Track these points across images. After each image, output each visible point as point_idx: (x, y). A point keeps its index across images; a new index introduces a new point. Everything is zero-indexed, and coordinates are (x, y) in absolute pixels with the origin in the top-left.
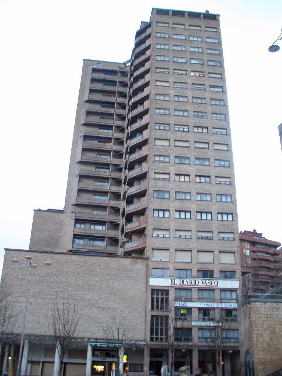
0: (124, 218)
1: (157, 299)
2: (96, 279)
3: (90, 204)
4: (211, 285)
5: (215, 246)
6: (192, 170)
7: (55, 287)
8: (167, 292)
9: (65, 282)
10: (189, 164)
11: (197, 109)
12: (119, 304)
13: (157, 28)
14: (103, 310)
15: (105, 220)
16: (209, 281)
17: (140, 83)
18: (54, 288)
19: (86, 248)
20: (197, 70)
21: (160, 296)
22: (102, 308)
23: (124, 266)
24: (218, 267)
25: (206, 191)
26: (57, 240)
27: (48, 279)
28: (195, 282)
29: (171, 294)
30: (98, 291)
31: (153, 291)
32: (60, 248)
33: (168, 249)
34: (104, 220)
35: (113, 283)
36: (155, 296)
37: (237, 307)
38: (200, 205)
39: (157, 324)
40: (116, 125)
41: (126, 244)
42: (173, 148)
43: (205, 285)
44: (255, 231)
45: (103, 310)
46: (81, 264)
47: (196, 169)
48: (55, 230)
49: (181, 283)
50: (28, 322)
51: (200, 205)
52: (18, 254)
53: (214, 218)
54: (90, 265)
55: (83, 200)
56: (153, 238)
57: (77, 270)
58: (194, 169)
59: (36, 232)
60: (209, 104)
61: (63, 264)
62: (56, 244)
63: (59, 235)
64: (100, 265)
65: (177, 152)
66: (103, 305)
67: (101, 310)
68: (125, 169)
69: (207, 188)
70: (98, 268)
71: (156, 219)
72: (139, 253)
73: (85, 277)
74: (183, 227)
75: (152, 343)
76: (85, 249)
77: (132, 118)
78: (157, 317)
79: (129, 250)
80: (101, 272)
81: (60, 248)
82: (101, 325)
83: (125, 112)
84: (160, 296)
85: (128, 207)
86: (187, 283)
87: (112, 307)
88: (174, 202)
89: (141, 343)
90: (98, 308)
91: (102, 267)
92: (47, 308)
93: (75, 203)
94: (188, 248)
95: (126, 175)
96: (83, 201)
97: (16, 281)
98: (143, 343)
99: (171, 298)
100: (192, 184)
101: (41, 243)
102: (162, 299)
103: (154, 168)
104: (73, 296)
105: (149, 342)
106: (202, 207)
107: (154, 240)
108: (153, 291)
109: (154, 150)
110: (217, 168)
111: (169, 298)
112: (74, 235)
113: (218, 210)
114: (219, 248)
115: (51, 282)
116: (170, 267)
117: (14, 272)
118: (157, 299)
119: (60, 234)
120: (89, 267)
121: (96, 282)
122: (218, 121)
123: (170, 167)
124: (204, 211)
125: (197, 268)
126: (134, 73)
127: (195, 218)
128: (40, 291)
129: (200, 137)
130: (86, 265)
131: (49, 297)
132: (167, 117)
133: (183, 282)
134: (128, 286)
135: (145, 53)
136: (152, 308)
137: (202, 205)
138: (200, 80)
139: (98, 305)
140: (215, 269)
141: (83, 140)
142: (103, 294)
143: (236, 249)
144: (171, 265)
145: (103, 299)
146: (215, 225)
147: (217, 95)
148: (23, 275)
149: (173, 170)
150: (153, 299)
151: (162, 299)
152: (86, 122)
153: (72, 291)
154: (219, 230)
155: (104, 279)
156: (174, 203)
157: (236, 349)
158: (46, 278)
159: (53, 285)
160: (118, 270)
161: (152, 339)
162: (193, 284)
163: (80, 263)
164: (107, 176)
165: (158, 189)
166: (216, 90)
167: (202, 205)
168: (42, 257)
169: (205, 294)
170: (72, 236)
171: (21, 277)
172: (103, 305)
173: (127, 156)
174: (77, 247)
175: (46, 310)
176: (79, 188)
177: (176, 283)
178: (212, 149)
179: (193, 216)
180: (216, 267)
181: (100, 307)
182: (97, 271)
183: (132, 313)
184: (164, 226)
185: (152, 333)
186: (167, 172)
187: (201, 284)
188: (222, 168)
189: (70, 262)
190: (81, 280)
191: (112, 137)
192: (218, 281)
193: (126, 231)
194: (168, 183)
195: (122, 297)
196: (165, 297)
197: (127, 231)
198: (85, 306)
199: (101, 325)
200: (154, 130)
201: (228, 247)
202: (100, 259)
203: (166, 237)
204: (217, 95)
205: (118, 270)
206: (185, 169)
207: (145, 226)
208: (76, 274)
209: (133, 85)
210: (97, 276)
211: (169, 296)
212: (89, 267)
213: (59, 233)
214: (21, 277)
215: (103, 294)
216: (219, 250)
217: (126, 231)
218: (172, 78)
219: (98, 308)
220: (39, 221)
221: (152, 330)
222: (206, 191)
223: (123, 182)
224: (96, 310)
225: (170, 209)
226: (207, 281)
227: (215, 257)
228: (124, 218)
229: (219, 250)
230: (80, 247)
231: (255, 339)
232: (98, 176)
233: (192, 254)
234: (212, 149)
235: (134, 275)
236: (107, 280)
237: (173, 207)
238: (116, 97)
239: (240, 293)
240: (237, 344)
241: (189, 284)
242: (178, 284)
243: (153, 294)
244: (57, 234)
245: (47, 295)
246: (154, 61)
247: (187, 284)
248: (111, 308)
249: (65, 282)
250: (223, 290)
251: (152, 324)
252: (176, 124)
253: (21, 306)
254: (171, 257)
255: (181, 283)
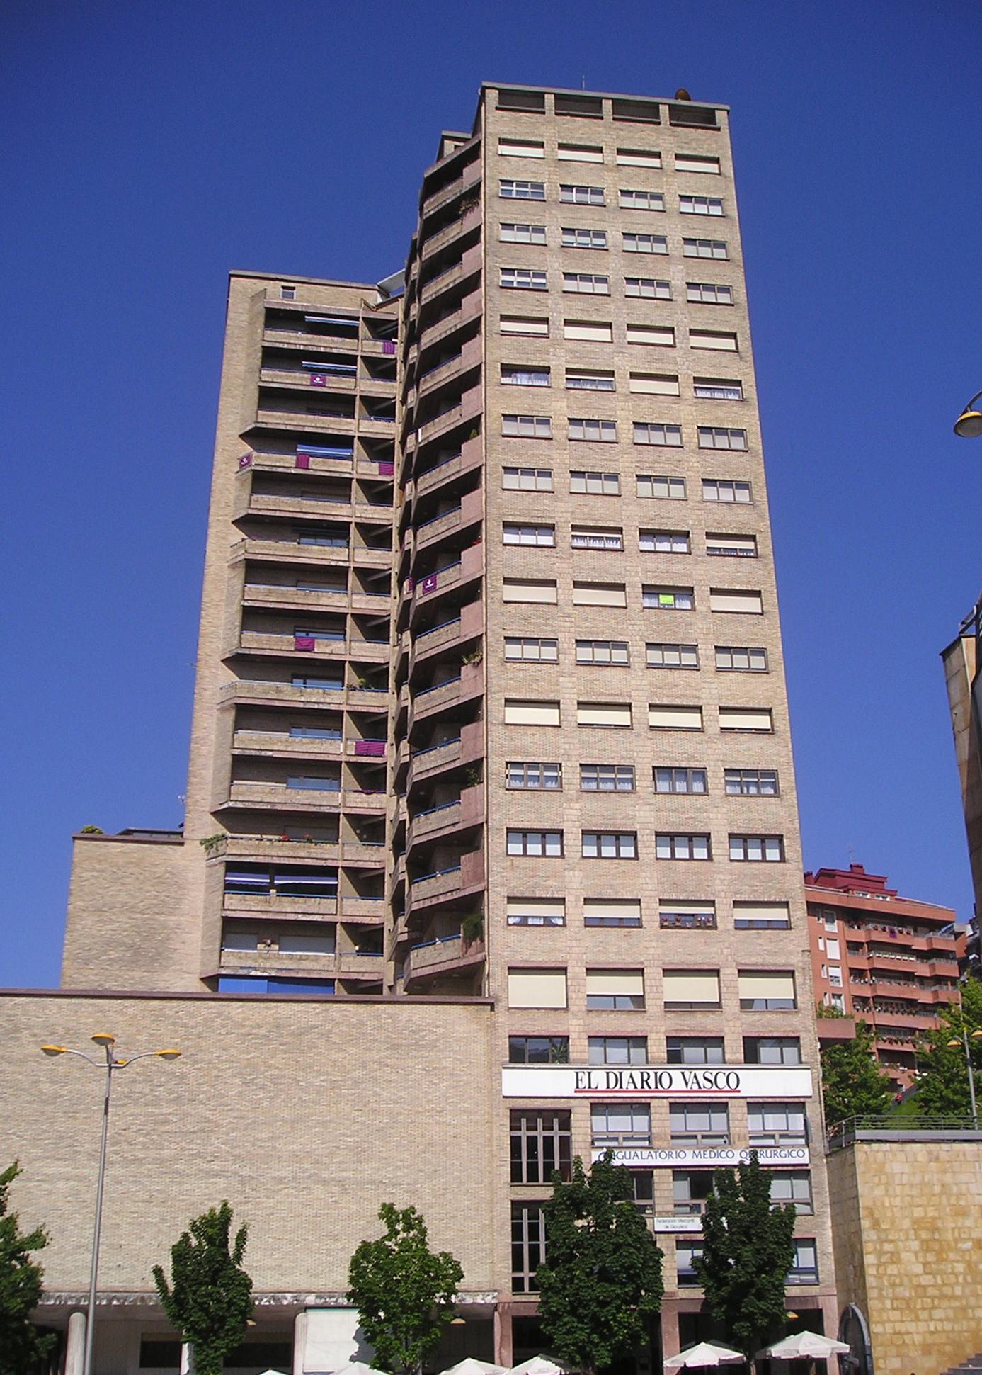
0: (403, 859)
1: (532, 1141)
2: (317, 1082)
3: (279, 807)
4: (714, 1088)
5: (725, 951)
6: (638, 685)
7: (170, 1117)
8: (564, 1117)
9: (208, 1099)
10: (626, 666)
11: (651, 468)
12: (398, 1168)
13: (503, 162)
14: (345, 1191)
15: (333, 864)
16: (708, 1075)
17: (445, 374)
18: (168, 1122)
19: (268, 965)
20: (648, 323)
21: (540, 1134)
22: (341, 1183)
23: (414, 1032)
24: (738, 1024)
25: (687, 760)
26: (161, 941)
27: (147, 1090)
28: (659, 1080)
29: (578, 1124)
30: (324, 1124)
31: (517, 1115)
32: (176, 971)
33: (563, 965)
34: (329, 863)
35: (376, 1094)
36: (524, 1134)
37: (806, 1160)
38: (668, 810)
39: (534, 1234)
40: (359, 520)
41: (413, 954)
42: (571, 610)
43: (695, 1087)
44: (381, 1216)
45: (345, 1191)
46: (263, 1031)
47: (651, 684)
48: (156, 905)
49: (612, 1084)
50: (80, 1247)
51: (668, 810)
52: (32, 1007)
53: (719, 852)
54: (292, 1034)
55: (252, 794)
56: (503, 941)
57: (248, 1053)
58: (644, 682)
59: (85, 915)
60: (694, 446)
61: (199, 1036)
62: (160, 954)
63: (171, 924)
64: (330, 1032)
65: (581, 624)
66: (344, 1174)
67: (336, 1189)
68: (400, 630)
69: (691, 751)
70: (321, 1043)
71: (517, 861)
72: (464, 984)
73: (278, 1077)
74: (612, 886)
75: (518, 1298)
76: (265, 969)
77: (421, 500)
78: (533, 1205)
79: (427, 971)
80: (335, 1055)
81: (176, 971)
82: (339, 1245)
83: (390, 430)
84: (540, 1134)
85: (415, 821)
86: (631, 1083)
87: (377, 1177)
88: (577, 801)
89: (479, 1300)
90: (325, 1182)
91: (334, 1038)
92: (146, 1197)
93: (226, 806)
94: (629, 962)
95: (404, 704)
96: (251, 799)
97: (29, 1102)
98: (489, 1299)
99: (580, 1138)
100: (639, 735)
101: (105, 952)
102: (548, 1141)
103: (503, 682)
104: (237, 1147)
105: (507, 1295)
106: (674, 818)
107: (515, 935)
108: (517, 1115)
109: (503, 619)
110: (723, 676)
111: (573, 1138)
112: (226, 920)
113: (731, 823)
114: (739, 960)
115: (157, 1102)
116: (572, 1028)
117: (20, 1074)
118: (532, 1141)
119: (172, 920)
120: (289, 1039)
121: (318, 1093)
122: (725, 507)
123: (561, 679)
124: (681, 829)
125: (663, 1029)
126: (422, 244)
127: (653, 856)
128: (120, 1134)
129: (662, 567)
130: (281, 1035)
131: (153, 1153)
132: (547, 499)
133: (619, 1080)
134: (428, 1101)
135: (461, 259)
136: (516, 1176)
137: (675, 810)
138: (660, 360)
139: (325, 1174)
140: (726, 1029)
141: (242, 576)
142: (344, 1135)
143: (795, 960)
144: (575, 1022)
145: (345, 1152)
146: (722, 877)
147: (720, 414)
148: (53, 1082)
149: (569, 688)
150: (515, 1142)
151: (548, 1141)
152: (250, 512)
153: (234, 1130)
154: (736, 893)
155: (345, 1081)
156: (577, 806)
157: (810, 1307)
158: (138, 1087)
159: (165, 1110)
160: (395, 1047)
161: (517, 1285)
162: (653, 1086)
163: (259, 1026)
164: (333, 707)
165: (519, 759)
166: (664, 546)
167: (675, 810)
168: (121, 1012)
169: (697, 1121)
170: (219, 924)
171: (46, 1087)
172: (344, 1174)
173: (409, 534)
174: (237, 964)
175: (143, 1201)
176: (236, 752)
177: (593, 1086)
178: (704, 609)
179: (644, 850)
180: (731, 1024)
181: (333, 1179)
182: (320, 1054)
183: (448, 1196)
184: (546, 888)
185: (517, 1266)
186: (551, 697)
187: (678, 1084)
188: (741, 676)
189: (224, 1026)
190: (263, 1087)
191: (347, 564)
192: (684, 1088)
193: (413, 840)
194: (556, 736)
195: (410, 1142)
196: (556, 1134)
197: (415, 907)
198: (281, 1180)
199: (339, 1245)
200: (500, 548)
201: (769, 953)
202: (327, 1010)
203: (557, 925)
204: (720, 414)
205: (395, 1047)
206: (611, 683)
207: (478, 888)
208: (246, 1067)
209: (420, 293)
210: (320, 1073)
211: (573, 1130)
212: (289, 1039)
213: (171, 914)
214: (46, 1087)
215: (344, 1135)
216: (738, 964)
217: (413, 840)
218: (562, 353)
219: (325, 1182)
220: (95, 874)
221: (517, 1253)
222: (687, 760)
223: (391, 726)
224: (318, 1190)
225: (565, 826)
226: (700, 1074)
227: (724, 990)
228: (403, 859)
229: (738, 964)
230: (248, 963)
231: (870, 1271)
232: (301, 705)
233: (647, 982)
234: (704, 609)
235: (447, 1063)
236: (356, 1083)
237: (575, 818)
238: (356, 416)
239: (816, 1112)
240: (814, 1290)
241: (639, 1086)
242: (603, 1087)
243: (515, 1126)
244: (161, 918)
245: (144, 1147)
246: (494, 292)
247: (631, 1087)
248: (373, 1182)
249: (208, 1099)
250: (759, 1106)
251: (516, 1232)
252: (578, 523)
253: (50, 1193)
254: (574, 996)
255: (612, 1084)
